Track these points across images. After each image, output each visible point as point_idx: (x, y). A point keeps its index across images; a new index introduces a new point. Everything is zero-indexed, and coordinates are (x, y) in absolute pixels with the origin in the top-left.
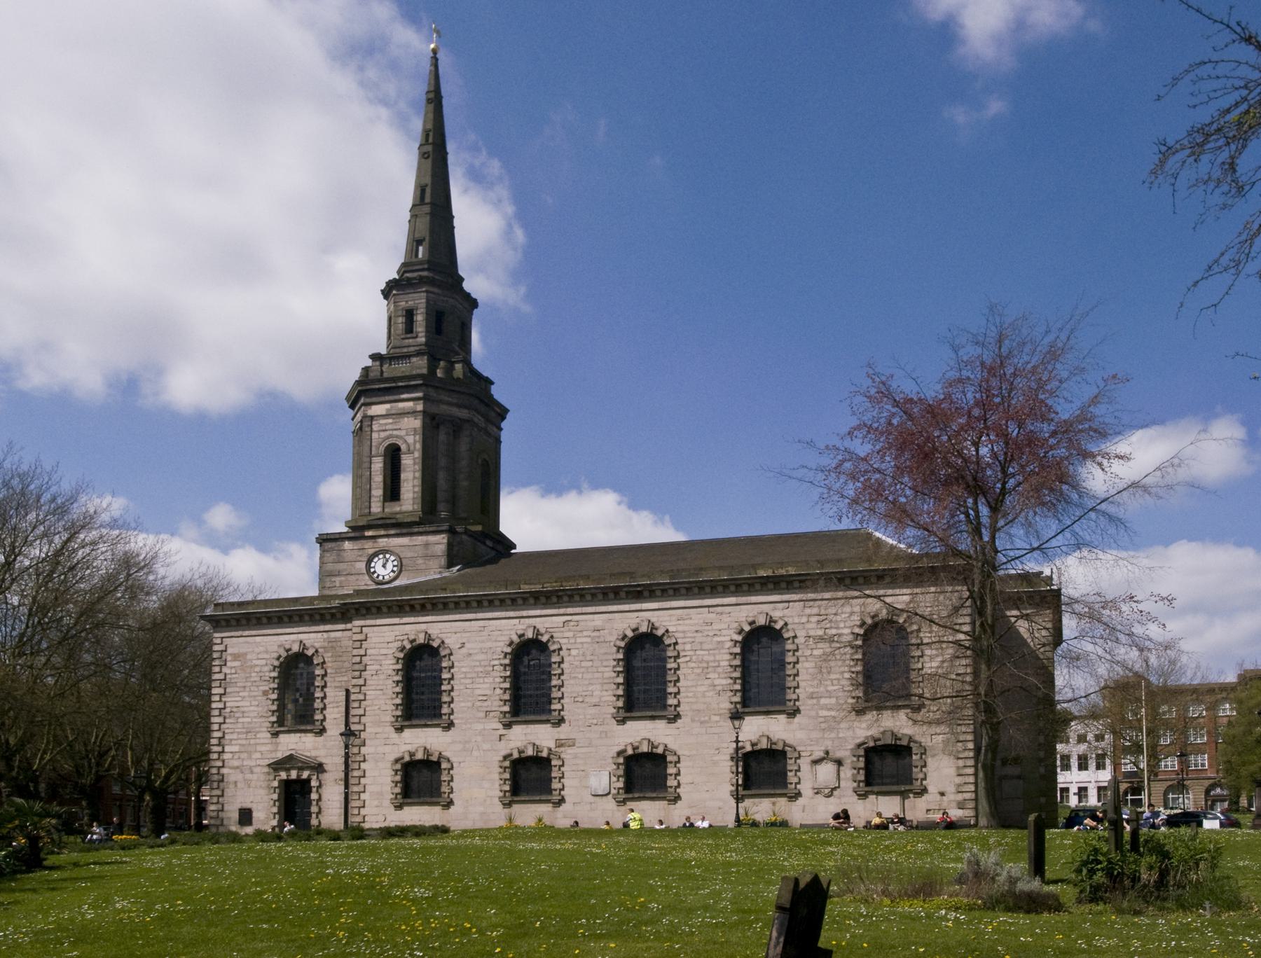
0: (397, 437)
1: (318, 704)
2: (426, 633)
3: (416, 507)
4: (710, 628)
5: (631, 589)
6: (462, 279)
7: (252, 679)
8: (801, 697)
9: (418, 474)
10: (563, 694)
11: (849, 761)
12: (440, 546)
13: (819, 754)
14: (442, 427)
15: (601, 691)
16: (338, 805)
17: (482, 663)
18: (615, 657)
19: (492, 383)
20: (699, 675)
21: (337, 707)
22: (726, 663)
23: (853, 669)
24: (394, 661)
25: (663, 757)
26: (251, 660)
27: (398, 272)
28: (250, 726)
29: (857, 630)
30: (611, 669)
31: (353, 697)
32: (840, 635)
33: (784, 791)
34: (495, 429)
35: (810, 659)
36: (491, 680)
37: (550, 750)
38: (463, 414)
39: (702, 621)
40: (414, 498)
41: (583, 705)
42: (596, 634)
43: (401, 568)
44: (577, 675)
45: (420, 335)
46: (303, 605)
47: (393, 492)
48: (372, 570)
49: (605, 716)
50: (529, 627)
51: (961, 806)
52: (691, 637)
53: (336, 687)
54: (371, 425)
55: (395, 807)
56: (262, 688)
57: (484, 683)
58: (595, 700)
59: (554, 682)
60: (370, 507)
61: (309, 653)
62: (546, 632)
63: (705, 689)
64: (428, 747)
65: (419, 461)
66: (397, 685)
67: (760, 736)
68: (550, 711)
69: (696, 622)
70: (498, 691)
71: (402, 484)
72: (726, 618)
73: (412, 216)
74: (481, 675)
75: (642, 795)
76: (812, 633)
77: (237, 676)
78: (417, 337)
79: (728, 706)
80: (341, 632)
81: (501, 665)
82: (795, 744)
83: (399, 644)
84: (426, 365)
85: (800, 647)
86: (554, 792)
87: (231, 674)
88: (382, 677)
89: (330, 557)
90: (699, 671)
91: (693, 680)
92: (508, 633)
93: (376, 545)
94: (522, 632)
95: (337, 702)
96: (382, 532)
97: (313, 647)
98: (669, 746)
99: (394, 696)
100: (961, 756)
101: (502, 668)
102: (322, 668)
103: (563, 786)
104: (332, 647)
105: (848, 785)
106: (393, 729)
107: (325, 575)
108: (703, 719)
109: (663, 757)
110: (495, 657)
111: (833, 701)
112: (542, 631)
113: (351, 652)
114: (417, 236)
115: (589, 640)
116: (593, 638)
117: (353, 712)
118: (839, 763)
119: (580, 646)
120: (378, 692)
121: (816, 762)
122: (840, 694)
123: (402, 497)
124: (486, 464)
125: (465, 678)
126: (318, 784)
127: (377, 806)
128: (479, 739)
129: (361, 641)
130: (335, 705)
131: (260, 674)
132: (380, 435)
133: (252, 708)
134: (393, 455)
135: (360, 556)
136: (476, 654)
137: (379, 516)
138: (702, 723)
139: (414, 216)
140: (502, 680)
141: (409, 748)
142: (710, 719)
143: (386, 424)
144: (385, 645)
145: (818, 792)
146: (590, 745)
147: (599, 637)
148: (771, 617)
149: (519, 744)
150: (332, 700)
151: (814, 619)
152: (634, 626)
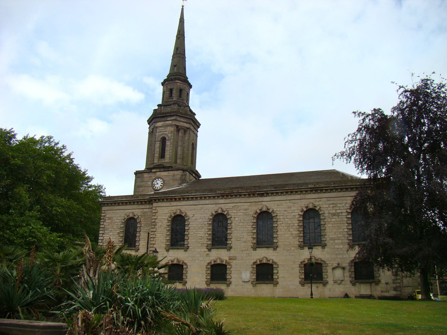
0: (165, 134)
2: (180, 210)
5: (260, 193)
6: (187, 78)
7: (114, 228)
8: (328, 239)
13: (335, 265)
15: (247, 236)
18: (253, 221)
21: (145, 240)
22: (297, 224)
25: (272, 265)
29: (349, 211)
30: (250, 226)
32: (342, 213)
33: (322, 282)
34: (196, 131)
35: (330, 223)
37: (226, 261)
38: (187, 125)
39: (287, 206)
40: (170, 157)
41: (240, 242)
42: (246, 211)
43: (164, 184)
44: (237, 229)
47: (162, 156)
50: (220, 208)
54: (156, 130)
56: (118, 231)
57: (201, 231)
58: (245, 240)
60: (154, 161)
61: (136, 217)
62: (226, 210)
64: (179, 258)
68: (227, 244)
74: (200, 228)
75: (263, 282)
76: (331, 212)
78: (172, 99)
79: (298, 243)
80: (148, 209)
81: (208, 224)
83: (169, 214)
86: (227, 280)
89: (139, 180)
90: (286, 228)
91: (283, 232)
93: (155, 175)
94: (216, 210)
95: (145, 238)
96: (158, 170)
97: (137, 215)
98: (274, 260)
103: (278, 277)
104: (144, 215)
105: (348, 279)
107: (136, 187)
108: (288, 249)
109: (272, 265)
110: (206, 221)
111: (340, 241)
112: (225, 210)
114: (175, 64)
115: (242, 214)
118: (344, 268)
119: (239, 216)
120: (162, 234)
121: (333, 269)
122: (343, 238)
124: (193, 144)
125: (194, 229)
130: (144, 239)
131: (117, 226)
132: (159, 135)
135: (150, 179)
136: (199, 219)
137: (158, 164)
138: (287, 250)
142: (291, 249)
145: (335, 282)
147: (246, 213)
149: (214, 258)
150: (143, 237)
151: (331, 206)
152: (260, 208)
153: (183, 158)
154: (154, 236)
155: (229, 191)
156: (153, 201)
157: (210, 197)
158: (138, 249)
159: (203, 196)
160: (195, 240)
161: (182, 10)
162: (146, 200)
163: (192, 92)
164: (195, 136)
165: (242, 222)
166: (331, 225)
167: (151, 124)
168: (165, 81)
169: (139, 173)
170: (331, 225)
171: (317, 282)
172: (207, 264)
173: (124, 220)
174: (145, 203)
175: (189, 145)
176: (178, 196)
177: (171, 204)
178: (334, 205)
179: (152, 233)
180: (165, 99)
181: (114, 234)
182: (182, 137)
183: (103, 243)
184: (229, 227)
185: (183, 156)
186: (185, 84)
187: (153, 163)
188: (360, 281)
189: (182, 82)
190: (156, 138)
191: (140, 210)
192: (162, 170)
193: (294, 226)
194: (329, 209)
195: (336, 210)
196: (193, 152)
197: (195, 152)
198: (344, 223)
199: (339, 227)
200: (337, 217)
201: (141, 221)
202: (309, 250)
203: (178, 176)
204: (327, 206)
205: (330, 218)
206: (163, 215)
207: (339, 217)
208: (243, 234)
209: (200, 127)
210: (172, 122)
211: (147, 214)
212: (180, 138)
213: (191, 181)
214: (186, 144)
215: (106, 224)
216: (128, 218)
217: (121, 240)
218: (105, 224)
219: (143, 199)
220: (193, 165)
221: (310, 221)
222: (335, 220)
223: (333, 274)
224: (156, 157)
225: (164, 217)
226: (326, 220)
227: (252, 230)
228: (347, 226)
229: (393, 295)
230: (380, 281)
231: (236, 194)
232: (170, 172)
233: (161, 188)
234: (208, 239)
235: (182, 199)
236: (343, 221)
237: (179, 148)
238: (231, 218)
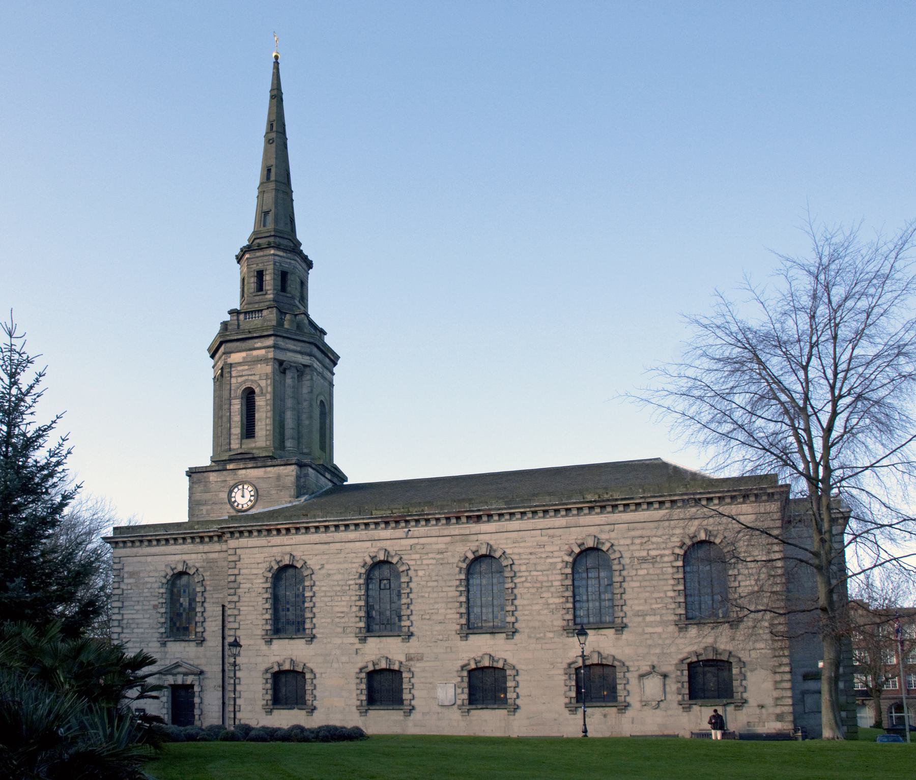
0: (252, 381)
1: (199, 618)
2: (291, 555)
3: (268, 443)
4: (543, 550)
5: (471, 514)
6: (300, 244)
7: (145, 595)
8: (629, 614)
9: (270, 414)
10: (412, 611)
11: (673, 676)
12: (289, 478)
14: (287, 372)
15: (446, 609)
16: (217, 710)
17: (340, 583)
18: (457, 577)
20: (534, 594)
21: (215, 621)
22: (557, 583)
23: (675, 588)
24: (263, 580)
26: (144, 578)
27: (249, 240)
28: (143, 636)
29: (678, 551)
30: (454, 589)
31: (229, 612)
32: (662, 556)
34: (329, 374)
35: (635, 578)
36: (348, 598)
38: (305, 360)
39: (535, 544)
40: (266, 435)
41: (430, 622)
42: (440, 556)
44: (423, 594)
45: (269, 292)
46: (186, 529)
47: (249, 431)
48: (233, 500)
49: (449, 633)
50: (380, 549)
51: (780, 717)
52: (525, 559)
53: (213, 603)
54: (230, 372)
55: (266, 712)
56: (152, 603)
57: (341, 601)
58: (440, 618)
59: (404, 601)
60: (230, 444)
62: (396, 554)
63: (540, 608)
64: (294, 659)
66: (267, 602)
67: (591, 652)
69: (529, 544)
70: (354, 609)
71: (256, 423)
72: (557, 541)
73: (259, 193)
74: (338, 594)
75: (484, 707)
76: (637, 554)
77: (131, 591)
78: (266, 294)
81: (356, 584)
82: (623, 660)
83: (266, 565)
85: (626, 567)
87: (127, 590)
88: (254, 594)
89: (199, 488)
90: (534, 590)
92: (362, 555)
95: (215, 617)
97: (194, 566)
99: (264, 611)
100: (778, 670)
101: (357, 586)
102: (202, 585)
103: (413, 696)
105: (673, 698)
106: (263, 641)
107: (194, 505)
108: (538, 636)
110: (351, 577)
111: (658, 618)
112: (393, 553)
114: (265, 209)
115: (434, 562)
116: (437, 560)
117: (228, 626)
118: (665, 676)
119: (426, 567)
121: (642, 676)
122: (664, 611)
123: (256, 434)
125: (325, 596)
126: (200, 690)
127: (251, 711)
128: (338, 652)
129: (235, 561)
131: (152, 590)
132: (237, 383)
133: (145, 621)
134: (249, 396)
135: (223, 487)
137: (239, 451)
139: (262, 192)
140: (357, 598)
141: (277, 659)
142: (545, 636)
143: (243, 370)
144: (256, 566)
145: (645, 704)
146: (436, 659)
147: (442, 559)
148: (598, 539)
151: (638, 541)
152: (474, 549)
153: (298, 438)
154: (236, 612)
155: (402, 510)
156: (229, 535)
157: (357, 525)
158: (204, 640)
159: (340, 523)
160: (329, 620)
162: (212, 534)
163: (314, 278)
164: (326, 384)
165: (433, 579)
166: (637, 584)
167: (217, 356)
168: (245, 250)
169: (196, 472)
170: (637, 584)
171: (604, 704)
172: (358, 670)
173: (165, 577)
174: (210, 541)
175: (311, 405)
176: (286, 524)
177: (269, 542)
178: (644, 540)
179: (229, 606)
180: (246, 296)
181: (146, 607)
182: (293, 387)
183: (123, 628)
184: (405, 592)
185: (299, 433)
187: (230, 450)
188: (700, 702)
189: (284, 255)
190: (230, 390)
191: (199, 555)
193: (552, 586)
194: (632, 548)
195: (648, 550)
196: (325, 423)
197: (328, 421)
198: (666, 580)
199: (654, 587)
200: (651, 565)
201: (204, 580)
202: (580, 637)
203: (289, 478)
204: (629, 542)
205: (634, 567)
206: (253, 566)
207: (656, 565)
208: (436, 606)
209: (339, 362)
210: (267, 352)
211: (216, 564)
212: (289, 392)
213: (322, 489)
214: (305, 404)
215: (125, 587)
216: (174, 574)
217: (163, 620)
219: (204, 532)
220: (325, 452)
221: (590, 575)
222: (645, 571)
223: (642, 689)
224: (235, 435)
225: (255, 571)
226: (624, 573)
227: (457, 597)
228: (673, 585)
229: (774, 731)
230: (746, 701)
231: (416, 518)
232: (269, 469)
233: (252, 507)
234: (357, 617)
235: (293, 531)
236: (663, 574)
237: (289, 415)
238: (409, 572)
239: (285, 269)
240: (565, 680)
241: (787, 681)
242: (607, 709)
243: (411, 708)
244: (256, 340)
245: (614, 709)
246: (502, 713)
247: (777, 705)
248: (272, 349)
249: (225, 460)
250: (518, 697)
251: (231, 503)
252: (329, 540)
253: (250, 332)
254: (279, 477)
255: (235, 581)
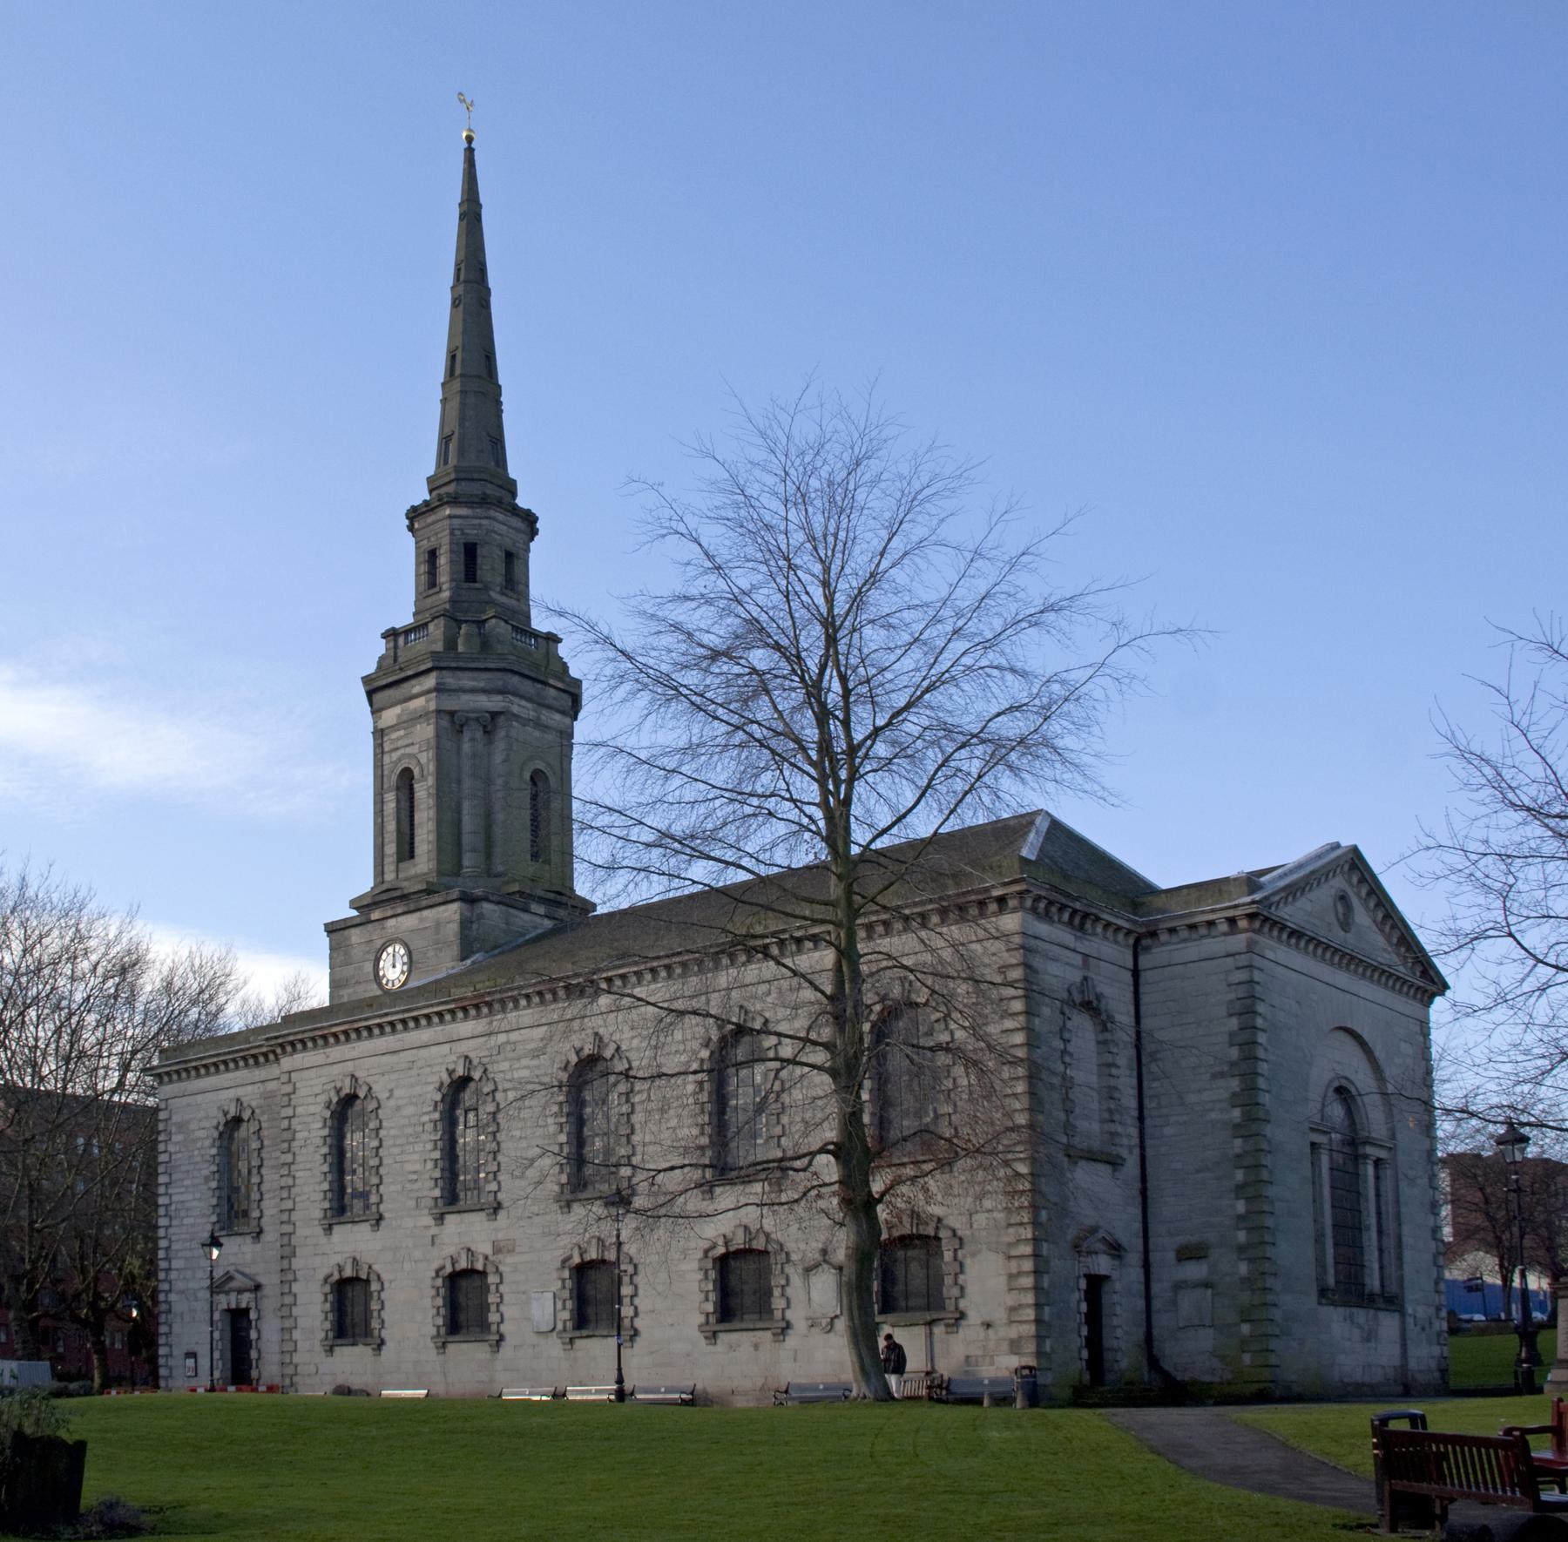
0: (410, 756)
12: (451, 925)
19: (560, 640)
37: (486, 1258)
47: (407, 850)
48: (381, 973)
57: (414, 1152)
65: (433, 791)
70: (430, 1165)
74: (411, 1140)
83: (323, 1098)
84: (442, 637)
100: (1014, 1252)
107: (335, 985)
113: (279, 1113)
141: (338, 1259)
143: (398, 739)
155: (487, 984)
161: (470, 152)
186: (484, 514)
191: (256, 1086)
192: (400, 910)
210: (427, 701)
218: (171, 1148)
232: (425, 913)
239: (471, 539)
240: (700, 1281)
241: (1027, 1273)
242: (758, 1334)
243: (784, 1325)
244: (413, 682)
245: (768, 1334)
246: (485, 1347)
247: (1012, 1322)
248: (434, 694)
249: (368, 906)
250: (636, 1314)
251: (377, 978)
252: (398, 1046)
253: (401, 669)
254: (438, 926)
255: (289, 1129)
